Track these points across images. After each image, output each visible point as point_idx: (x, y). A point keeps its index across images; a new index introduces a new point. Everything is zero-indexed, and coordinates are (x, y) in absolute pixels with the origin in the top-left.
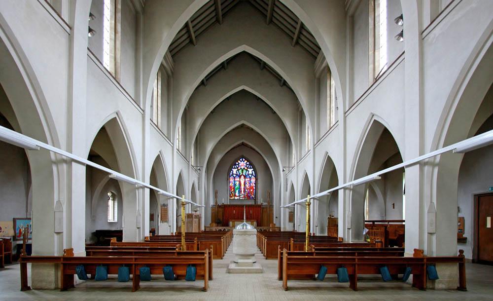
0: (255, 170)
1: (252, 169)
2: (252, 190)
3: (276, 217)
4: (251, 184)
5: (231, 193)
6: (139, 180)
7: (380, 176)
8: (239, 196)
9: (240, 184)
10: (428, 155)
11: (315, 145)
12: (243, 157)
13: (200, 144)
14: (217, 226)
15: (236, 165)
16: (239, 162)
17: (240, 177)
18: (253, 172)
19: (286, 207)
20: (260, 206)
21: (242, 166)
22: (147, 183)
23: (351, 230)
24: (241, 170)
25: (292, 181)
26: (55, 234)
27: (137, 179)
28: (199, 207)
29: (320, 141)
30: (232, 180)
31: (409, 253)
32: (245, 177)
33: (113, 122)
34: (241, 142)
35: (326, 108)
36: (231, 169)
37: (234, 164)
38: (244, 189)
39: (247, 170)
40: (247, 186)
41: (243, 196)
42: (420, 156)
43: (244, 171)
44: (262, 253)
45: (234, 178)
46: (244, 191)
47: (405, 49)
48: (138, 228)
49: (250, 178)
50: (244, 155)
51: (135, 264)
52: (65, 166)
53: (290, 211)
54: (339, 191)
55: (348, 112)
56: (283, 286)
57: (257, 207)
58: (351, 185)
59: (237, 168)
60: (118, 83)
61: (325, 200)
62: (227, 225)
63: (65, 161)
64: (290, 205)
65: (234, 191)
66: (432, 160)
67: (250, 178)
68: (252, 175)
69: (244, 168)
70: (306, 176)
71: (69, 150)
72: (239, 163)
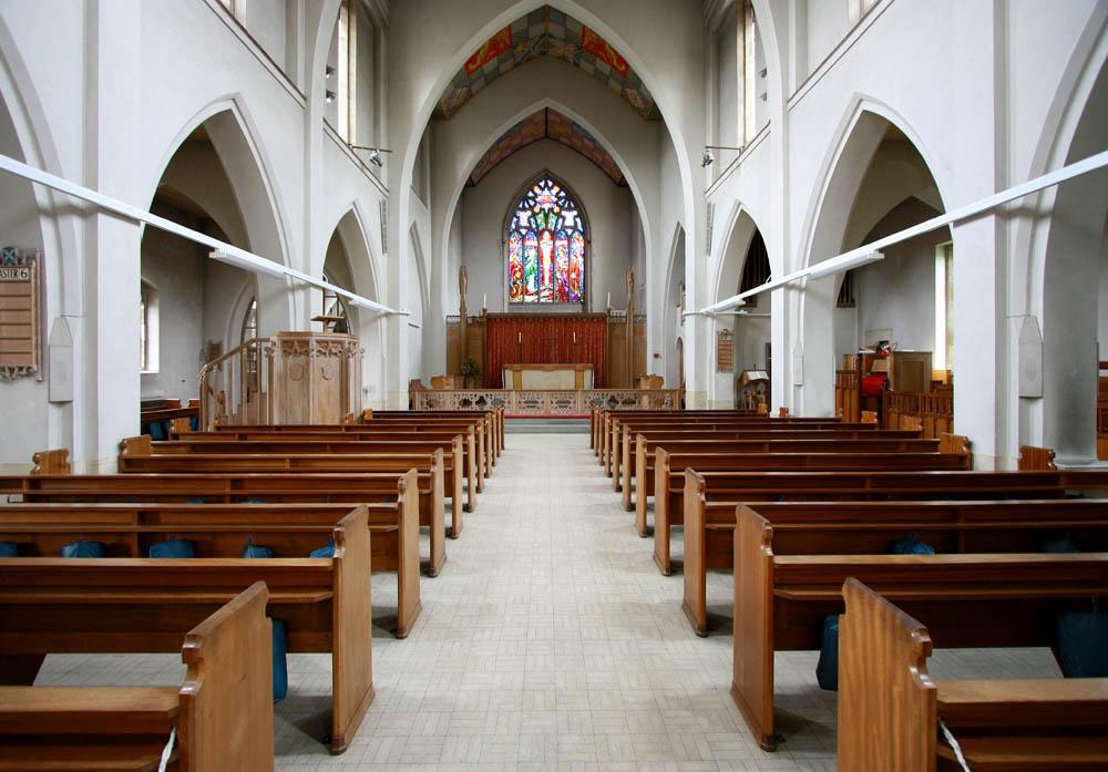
0: (582, 215)
1: (575, 213)
2: (573, 276)
3: (656, 356)
4: (572, 257)
5: (515, 283)
6: (296, 269)
7: (881, 250)
8: (537, 296)
9: (540, 258)
10: (1015, 193)
11: (788, 101)
12: (547, 176)
13: (389, 80)
14: (465, 387)
16: (537, 190)
17: (539, 234)
18: (578, 220)
19: (708, 315)
20: (601, 319)
21: (544, 202)
22: (317, 276)
23: (1038, 409)
24: (542, 215)
25: (231, 599)
26: (51, 407)
27: (290, 267)
28: (388, 315)
30: (515, 245)
31: (775, 413)
32: (554, 235)
33: (224, 120)
36: (511, 213)
37: (522, 198)
38: (552, 272)
39: (559, 215)
41: (547, 293)
42: (996, 192)
43: (552, 219)
44: (603, 464)
45: (523, 238)
46: (552, 279)
47: (771, 117)
48: (61, 404)
49: (569, 238)
50: (556, 171)
51: (141, 535)
52: (76, 224)
53: (721, 328)
54: (773, 293)
55: (795, 100)
56: (686, 606)
57: (586, 320)
58: (1041, 191)
59: (531, 208)
60: (295, 88)
61: (831, 291)
62: (497, 383)
63: (72, 210)
64: (719, 305)
66: (1032, 202)
67: (569, 238)
68: (574, 228)
69: (551, 210)
71: (91, 181)
72: (536, 195)
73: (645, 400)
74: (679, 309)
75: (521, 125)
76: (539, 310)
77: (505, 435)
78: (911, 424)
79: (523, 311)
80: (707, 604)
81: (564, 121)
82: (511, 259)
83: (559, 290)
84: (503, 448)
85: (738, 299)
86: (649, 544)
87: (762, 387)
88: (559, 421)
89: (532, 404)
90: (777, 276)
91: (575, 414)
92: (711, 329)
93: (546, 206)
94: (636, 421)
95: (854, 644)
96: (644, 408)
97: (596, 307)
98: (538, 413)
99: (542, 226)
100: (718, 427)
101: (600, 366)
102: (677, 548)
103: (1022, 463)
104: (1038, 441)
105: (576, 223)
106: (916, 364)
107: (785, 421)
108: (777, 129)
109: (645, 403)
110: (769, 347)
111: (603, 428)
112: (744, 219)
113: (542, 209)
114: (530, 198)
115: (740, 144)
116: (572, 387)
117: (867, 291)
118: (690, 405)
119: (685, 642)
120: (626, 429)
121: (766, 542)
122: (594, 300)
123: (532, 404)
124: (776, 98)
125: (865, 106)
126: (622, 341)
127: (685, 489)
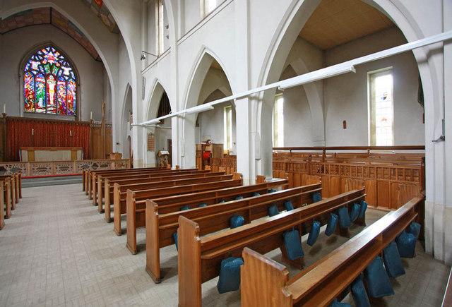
0: (74, 70)
3: (118, 144)
4: (69, 92)
5: (28, 101)
9: (47, 89)
12: (52, 46)
15: (38, 55)
17: (46, 76)
18: (72, 73)
19: (144, 126)
20: (87, 125)
23: (260, 163)
29: (206, 20)
30: (28, 79)
31: (174, 168)
32: (56, 78)
34: (49, 5)
35: (155, 42)
36: (26, 60)
37: (34, 53)
39: (60, 68)
40: (61, 94)
41: (52, 109)
46: (55, 101)
49: (66, 81)
57: (77, 124)
59: (41, 61)
61: (194, 120)
62: (16, 158)
64: (148, 122)
68: (70, 76)
73: (113, 164)
74: (129, 123)
75: (24, 14)
76: (46, 118)
77: (22, 189)
78: (222, 170)
79: (35, 117)
80: (161, 263)
81: (62, 18)
82: (26, 87)
83: (60, 108)
84: (20, 197)
85: (157, 120)
86: (124, 238)
87: (166, 157)
88: (61, 176)
89: (43, 169)
90: (174, 111)
91: (71, 173)
92: (145, 132)
93: (51, 62)
94: (112, 175)
95: (250, 280)
96: (112, 169)
97: (83, 119)
98: (47, 174)
99: (48, 72)
100: (152, 176)
101: (87, 148)
102: (124, 225)
103: (257, 181)
104: (260, 174)
105: (71, 74)
106: (219, 148)
107: (178, 171)
108: (173, 50)
109: (113, 166)
110: (170, 142)
111: (92, 180)
112: (159, 86)
113: (47, 63)
114: (40, 55)
115: (157, 54)
116: (70, 159)
117: (204, 120)
118: (136, 166)
119: (150, 290)
120: (106, 181)
121: (156, 211)
122: (82, 115)
123: (43, 169)
124: (172, 39)
125: (206, 51)
126: (99, 137)
127: (146, 209)
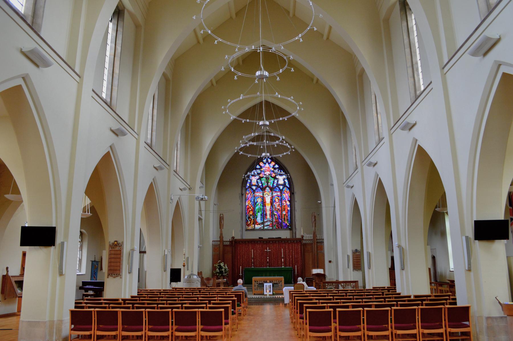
2: (284, 213)
5: (249, 218)
9: (264, 203)
11: (443, 68)
16: (261, 164)
17: (263, 189)
18: (286, 181)
39: (275, 178)
43: (271, 181)
46: (272, 215)
49: (281, 191)
65: (254, 215)
68: (284, 185)
70: (380, 184)
72: (261, 167)
